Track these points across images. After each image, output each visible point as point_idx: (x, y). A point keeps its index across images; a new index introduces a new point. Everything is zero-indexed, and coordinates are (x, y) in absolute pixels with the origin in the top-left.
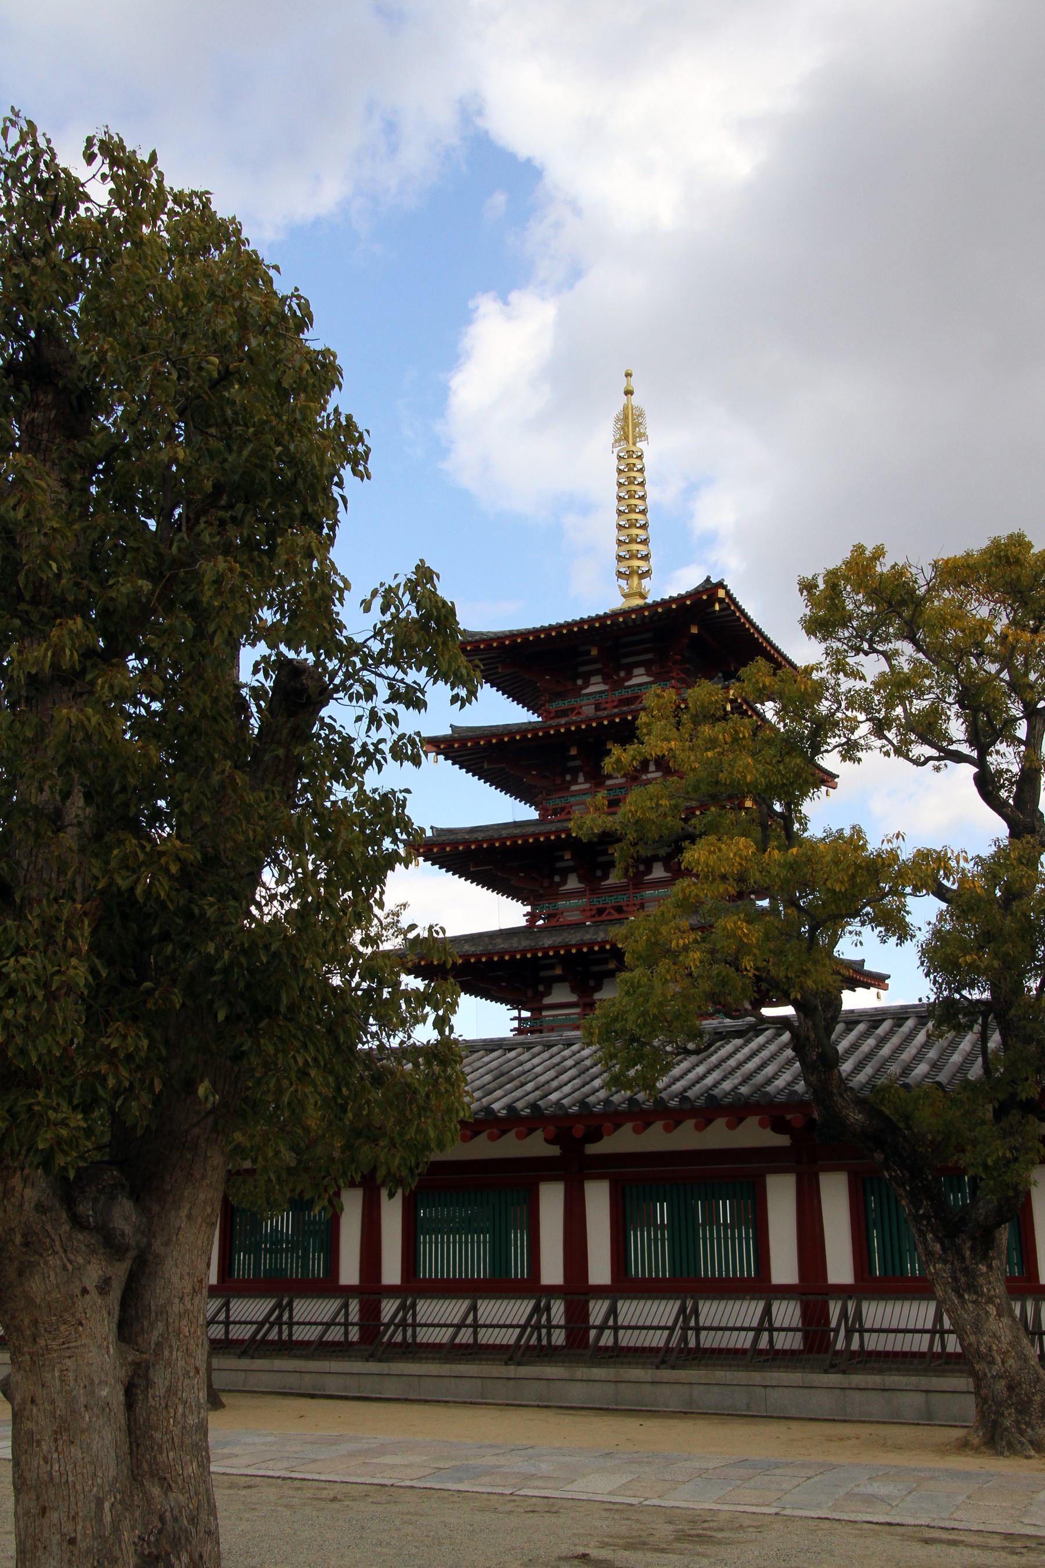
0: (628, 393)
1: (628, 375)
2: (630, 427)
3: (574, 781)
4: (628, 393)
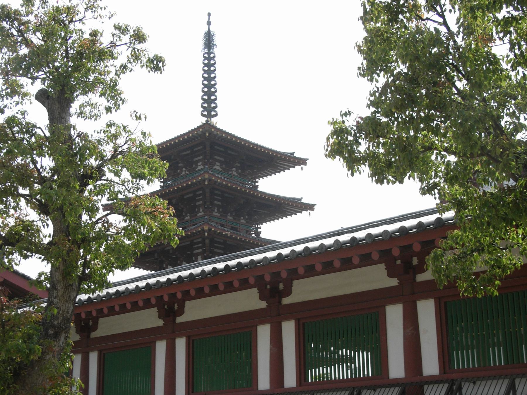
0: (209, 23)
1: (209, 14)
2: (209, 41)
3: (199, 212)
4: (209, 23)
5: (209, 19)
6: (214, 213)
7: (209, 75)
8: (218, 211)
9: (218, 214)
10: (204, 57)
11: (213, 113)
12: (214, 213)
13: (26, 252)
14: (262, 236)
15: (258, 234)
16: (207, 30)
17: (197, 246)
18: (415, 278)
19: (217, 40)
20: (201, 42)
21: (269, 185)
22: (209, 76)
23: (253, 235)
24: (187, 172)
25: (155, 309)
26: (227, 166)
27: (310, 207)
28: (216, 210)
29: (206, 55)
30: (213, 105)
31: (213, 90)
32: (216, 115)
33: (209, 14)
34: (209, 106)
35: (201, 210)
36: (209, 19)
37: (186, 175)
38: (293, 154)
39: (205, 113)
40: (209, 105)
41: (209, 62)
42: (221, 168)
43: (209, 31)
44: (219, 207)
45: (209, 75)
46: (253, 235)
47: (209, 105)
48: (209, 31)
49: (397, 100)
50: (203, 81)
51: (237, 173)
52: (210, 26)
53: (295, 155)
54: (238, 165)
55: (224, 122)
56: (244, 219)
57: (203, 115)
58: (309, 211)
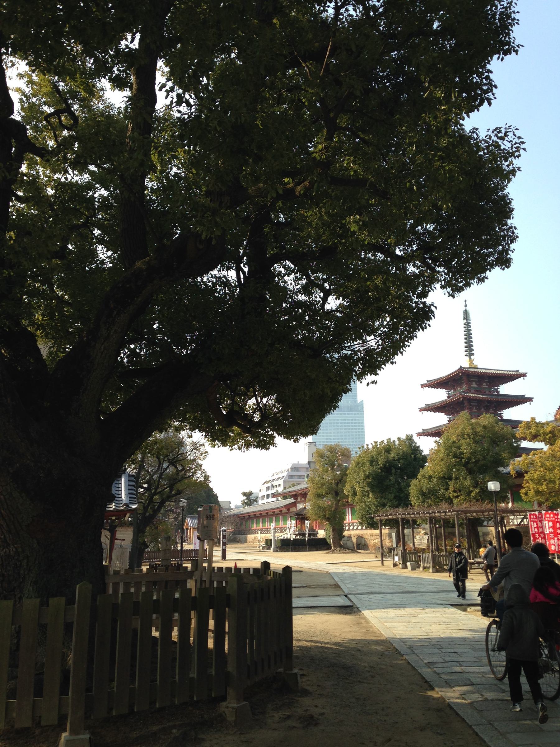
0: (466, 306)
1: (466, 301)
2: (466, 315)
4: (466, 306)
20: (462, 316)
33: (466, 301)
38: (517, 371)
40: (470, 351)
43: (466, 310)
47: (470, 351)
48: (466, 310)
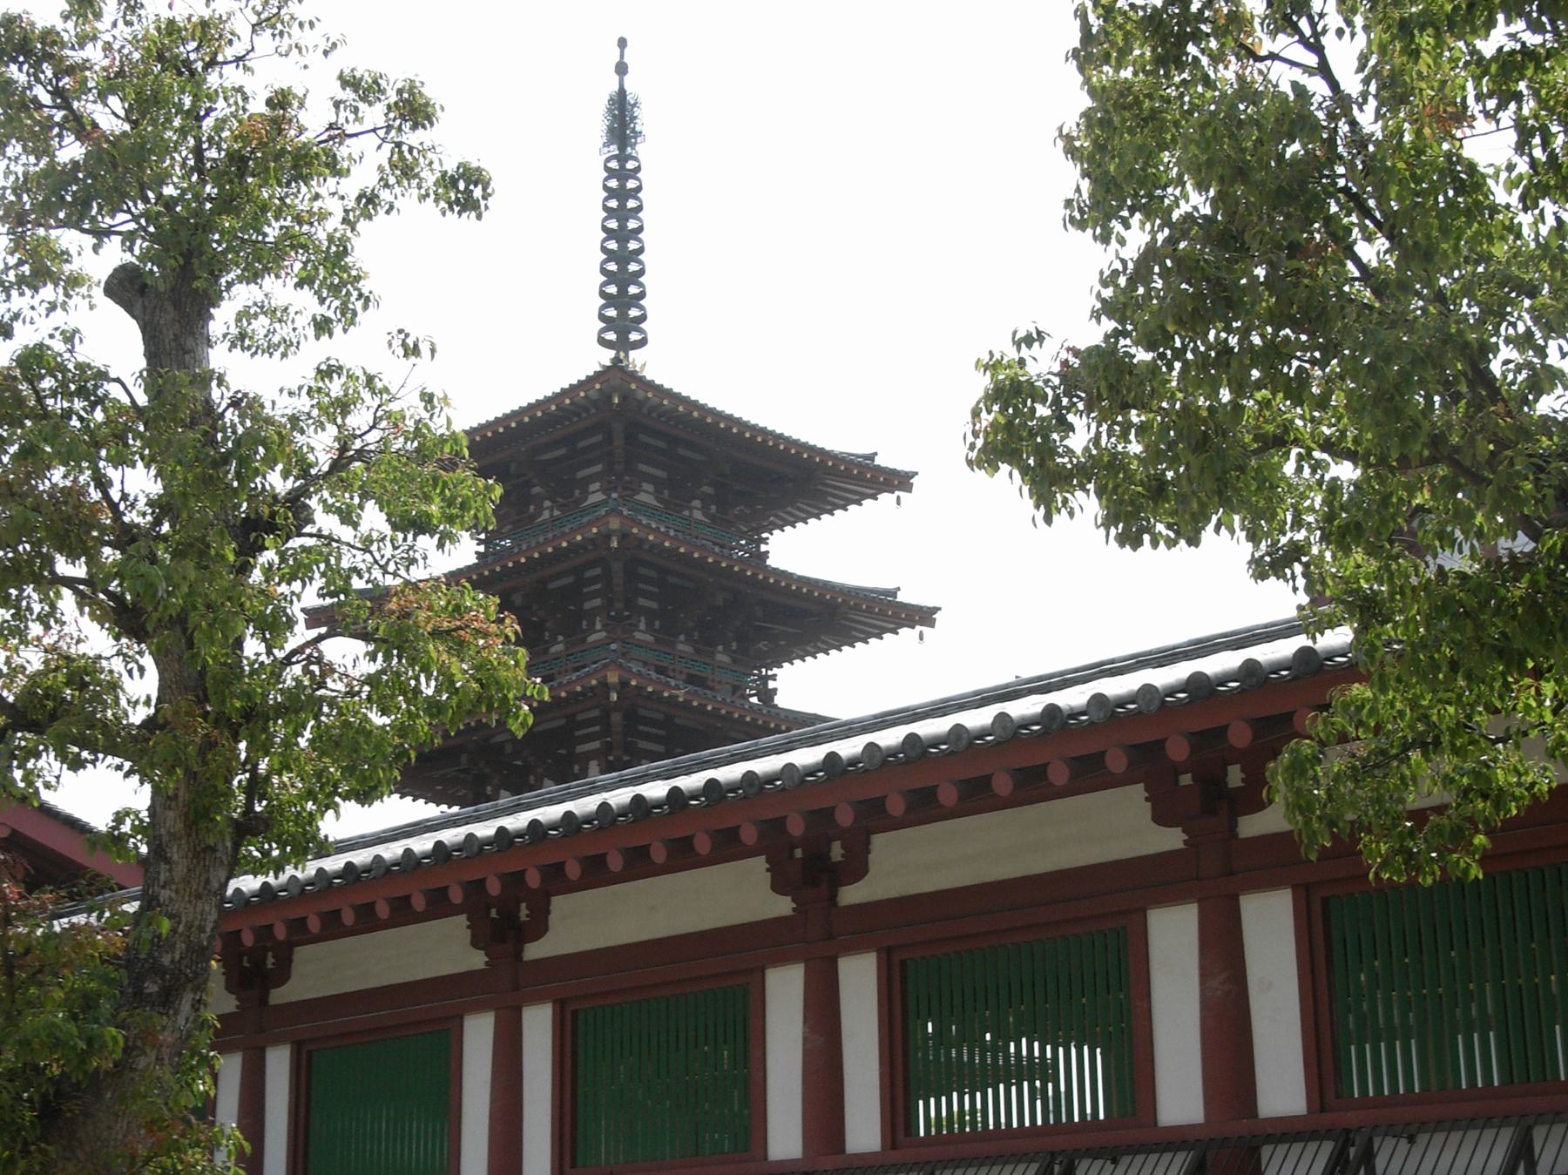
0: (622, 69)
1: (622, 43)
2: (622, 123)
3: (592, 630)
4: (622, 69)
5: (622, 56)
6: (638, 635)
7: (623, 223)
8: (650, 629)
9: (649, 638)
10: (607, 169)
11: (634, 336)
12: (638, 635)
13: (76, 750)
14: (781, 701)
15: (767, 696)
16: (616, 88)
17: (585, 731)
18: (1233, 826)
19: (645, 120)
20: (597, 124)
21: (802, 550)
22: (622, 226)
23: (754, 700)
24: (556, 513)
25: (462, 919)
26: (676, 492)
27: (923, 616)
28: (642, 626)
29: (614, 164)
30: (634, 313)
31: (633, 267)
32: (643, 342)
33: (622, 43)
34: (623, 314)
35: (598, 626)
36: (622, 56)
37: (553, 519)
39: (611, 336)
40: (622, 311)
41: (622, 186)
42: (657, 499)
43: (622, 93)
44: (651, 615)
45: (623, 223)
46: (754, 700)
47: (622, 311)
48: (622, 93)
49: (1180, 296)
50: (604, 240)
51: (704, 514)
52: (626, 78)
53: (878, 461)
54: (709, 490)
55: (666, 363)
56: (727, 651)
57: (603, 342)
58: (918, 628)
